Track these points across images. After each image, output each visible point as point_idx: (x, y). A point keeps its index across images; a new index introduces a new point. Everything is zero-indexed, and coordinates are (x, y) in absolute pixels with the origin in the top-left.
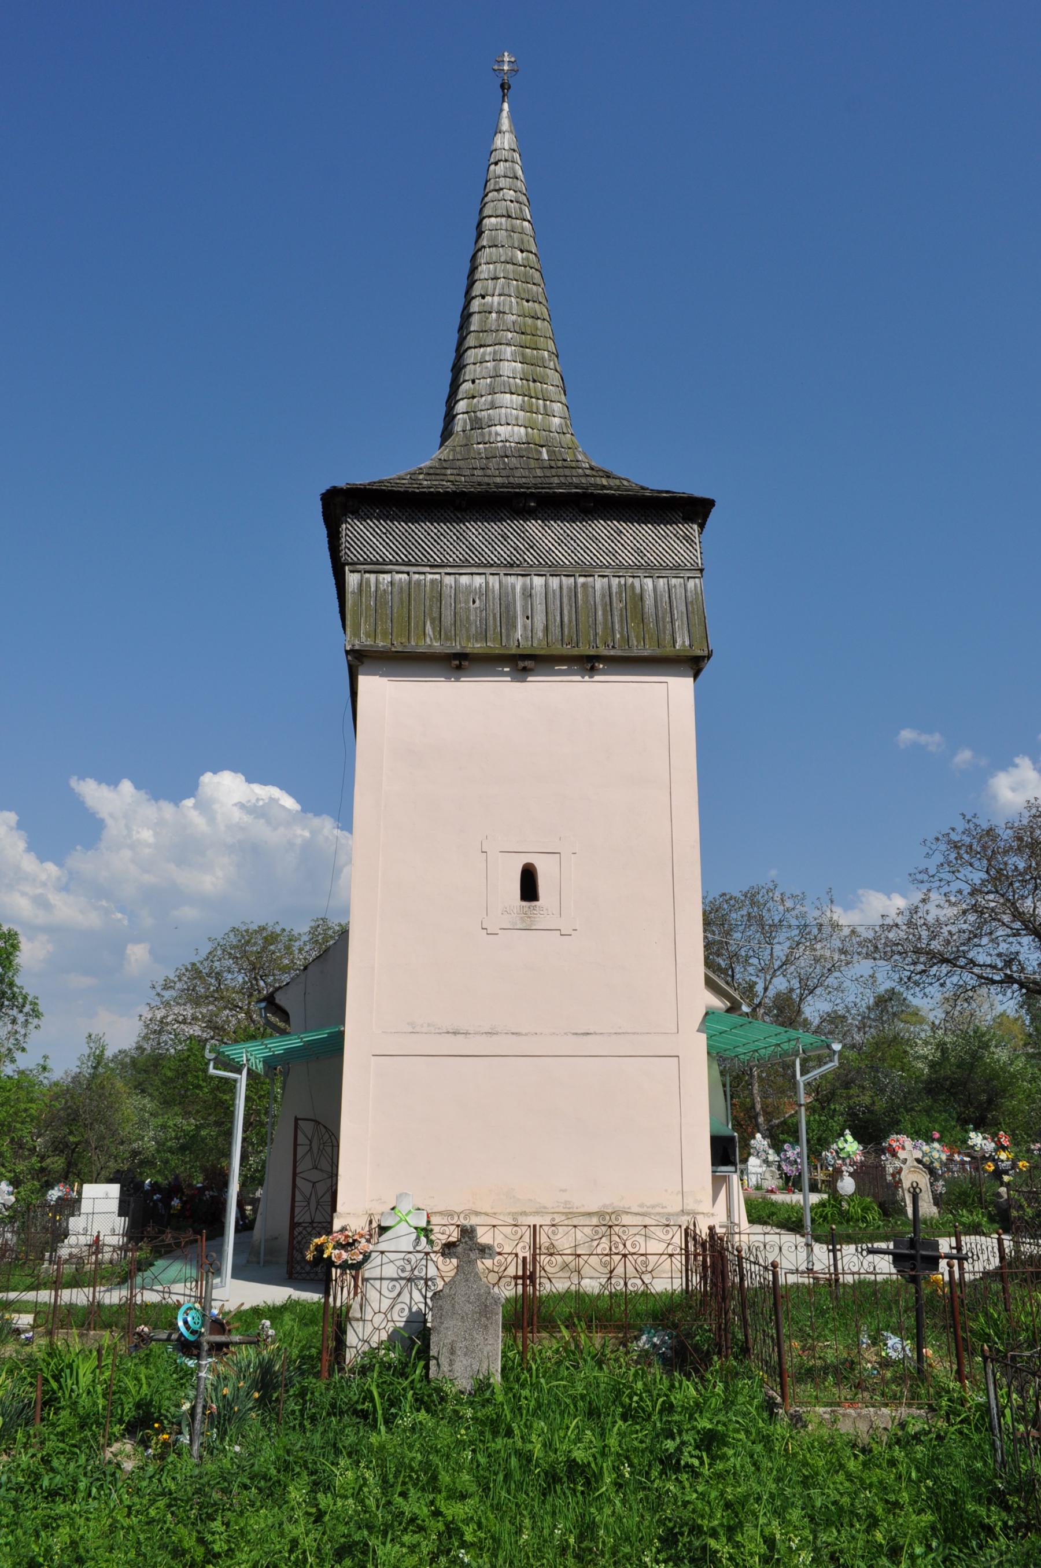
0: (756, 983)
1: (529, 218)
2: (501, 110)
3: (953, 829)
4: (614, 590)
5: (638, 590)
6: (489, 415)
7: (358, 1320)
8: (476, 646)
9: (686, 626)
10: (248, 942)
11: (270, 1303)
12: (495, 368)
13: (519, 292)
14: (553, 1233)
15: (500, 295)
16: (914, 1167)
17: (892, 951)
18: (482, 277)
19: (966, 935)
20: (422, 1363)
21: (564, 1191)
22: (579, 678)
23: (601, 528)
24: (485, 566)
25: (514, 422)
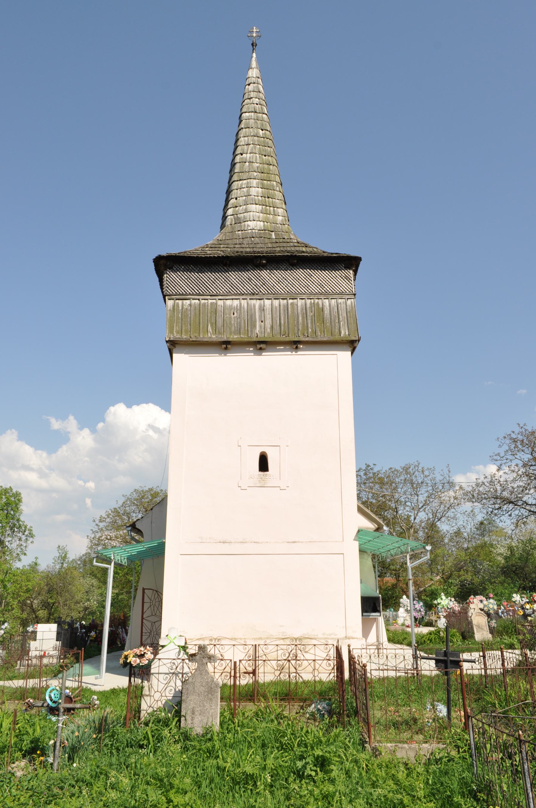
0: (411, 516)
1: (266, 112)
2: (252, 57)
3: (513, 432)
4: (308, 306)
5: (321, 306)
6: (244, 216)
7: (147, 696)
8: (234, 337)
9: (346, 324)
10: (143, 497)
11: (121, 687)
12: (248, 191)
13: (260, 151)
14: (266, 648)
15: (250, 153)
16: (479, 613)
17: (481, 497)
18: (241, 144)
19: (521, 489)
20: (176, 719)
21: (282, 626)
22: (289, 353)
23: (300, 273)
24: (239, 295)
25: (257, 219)
